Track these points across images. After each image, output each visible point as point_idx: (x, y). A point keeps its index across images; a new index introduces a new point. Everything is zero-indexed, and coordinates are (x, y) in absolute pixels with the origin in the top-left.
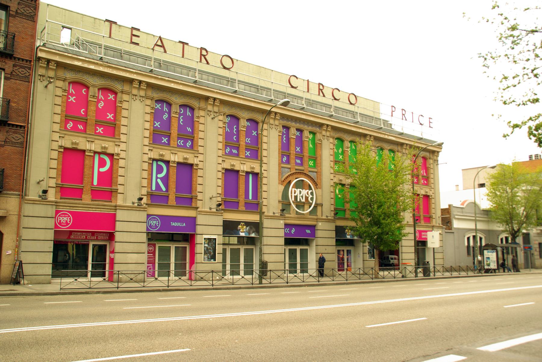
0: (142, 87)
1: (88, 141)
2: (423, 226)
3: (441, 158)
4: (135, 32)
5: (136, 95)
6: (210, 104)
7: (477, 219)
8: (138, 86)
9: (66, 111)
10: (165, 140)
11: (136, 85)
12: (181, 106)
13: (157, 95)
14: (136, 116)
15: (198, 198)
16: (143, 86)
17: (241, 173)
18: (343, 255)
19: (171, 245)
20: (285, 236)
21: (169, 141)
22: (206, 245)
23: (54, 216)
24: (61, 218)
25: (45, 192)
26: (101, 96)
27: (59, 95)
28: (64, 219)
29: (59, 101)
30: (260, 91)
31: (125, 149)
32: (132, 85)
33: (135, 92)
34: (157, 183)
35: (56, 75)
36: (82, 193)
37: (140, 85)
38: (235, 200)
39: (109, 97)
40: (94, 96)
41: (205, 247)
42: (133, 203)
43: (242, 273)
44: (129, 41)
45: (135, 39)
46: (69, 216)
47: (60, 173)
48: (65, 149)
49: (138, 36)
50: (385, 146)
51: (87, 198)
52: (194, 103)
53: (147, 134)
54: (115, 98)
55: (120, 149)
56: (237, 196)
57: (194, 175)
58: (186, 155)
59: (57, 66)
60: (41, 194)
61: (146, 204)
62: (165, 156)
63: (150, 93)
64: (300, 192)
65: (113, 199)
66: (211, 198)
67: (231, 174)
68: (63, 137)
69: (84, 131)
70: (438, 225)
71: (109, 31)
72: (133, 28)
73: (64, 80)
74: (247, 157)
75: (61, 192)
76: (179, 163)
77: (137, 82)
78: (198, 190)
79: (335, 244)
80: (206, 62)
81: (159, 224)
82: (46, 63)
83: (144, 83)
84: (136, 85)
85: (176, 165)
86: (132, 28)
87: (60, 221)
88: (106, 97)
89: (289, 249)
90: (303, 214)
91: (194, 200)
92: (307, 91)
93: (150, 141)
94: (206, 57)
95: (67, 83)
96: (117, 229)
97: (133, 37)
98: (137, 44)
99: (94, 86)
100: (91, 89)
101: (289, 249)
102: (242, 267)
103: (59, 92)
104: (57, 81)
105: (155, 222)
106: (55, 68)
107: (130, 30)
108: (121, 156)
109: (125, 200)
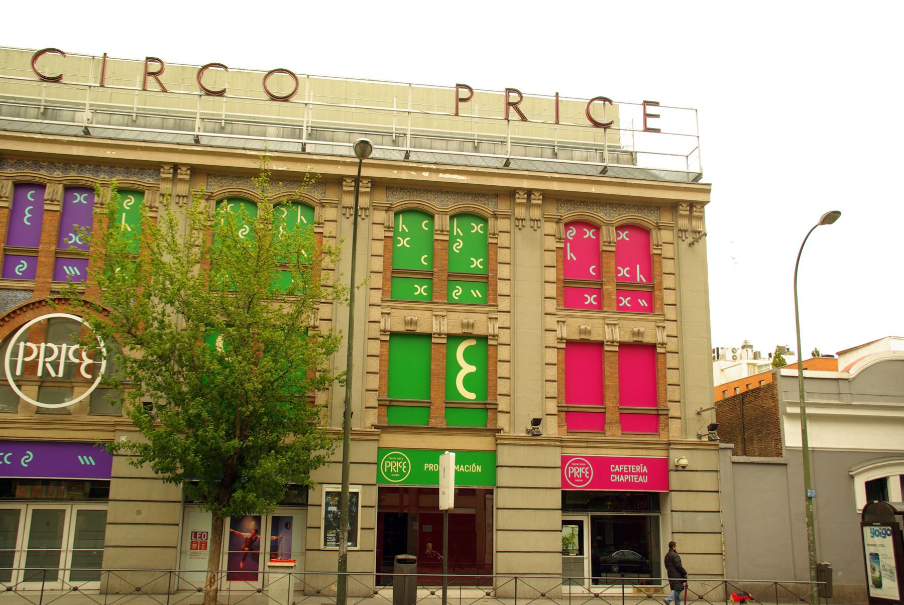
0: (179, 176)
1: (490, 318)
2: (617, 444)
3: (715, 218)
4: (650, 110)
5: (685, 231)
6: (683, 216)
7: (809, 411)
8: (688, 213)
9: (565, 274)
10: (591, 299)
11: (521, 199)
12: (621, 228)
13: (568, 213)
14: (530, 260)
15: (500, 408)
16: (537, 200)
17: (606, 348)
18: (257, 531)
19: (67, 507)
20: (563, 487)
21: (599, 300)
22: (334, 509)
23: (560, 465)
24: (574, 469)
25: (536, 422)
26: (456, 230)
27: (551, 248)
28: (578, 471)
29: (551, 258)
30: (229, 127)
31: (674, 334)
32: (159, 172)
33: (520, 212)
34: (44, 367)
35: (371, 203)
36: (604, 422)
37: (691, 211)
38: (595, 408)
39: (586, 234)
40: (442, 231)
41: (327, 512)
42: (700, 436)
43: (64, 575)
44: (642, 128)
45: (652, 123)
46: (587, 465)
47: (563, 387)
48: (393, 334)
49: (657, 116)
50: (434, 203)
51: (614, 431)
52: (648, 219)
53: (551, 290)
54: (485, 229)
55: (497, 325)
56: (601, 400)
57: (660, 366)
58: (640, 326)
59: (543, 199)
60: (530, 427)
61: (376, 427)
62: (594, 332)
63: (552, 210)
64: (49, 352)
65: (661, 428)
66: (699, 414)
67: (581, 355)
68: (389, 314)
69: (599, 307)
70: (694, 439)
71: (554, 114)
72: (646, 103)
73: (388, 210)
74: (622, 309)
75: (567, 421)
76: (622, 345)
77: (522, 193)
78: (670, 396)
79: (559, 506)
80: (159, 89)
81: (589, 475)
82: (526, 196)
83: (537, 194)
84: (521, 199)
85: (617, 349)
86: (645, 102)
87: (573, 474)
88: (467, 231)
89: (80, 512)
90: (65, 412)
91: (662, 418)
92: (553, 120)
93: (558, 305)
94: (519, 106)
95: (392, 214)
96: (114, 473)
97: (648, 119)
98: (657, 131)
99: (609, 224)
100: (604, 229)
101: (80, 512)
102: (66, 560)
103: (552, 243)
104: (375, 212)
105: (581, 470)
106: (540, 202)
107: (642, 107)
108: (669, 348)
109: (512, 424)
